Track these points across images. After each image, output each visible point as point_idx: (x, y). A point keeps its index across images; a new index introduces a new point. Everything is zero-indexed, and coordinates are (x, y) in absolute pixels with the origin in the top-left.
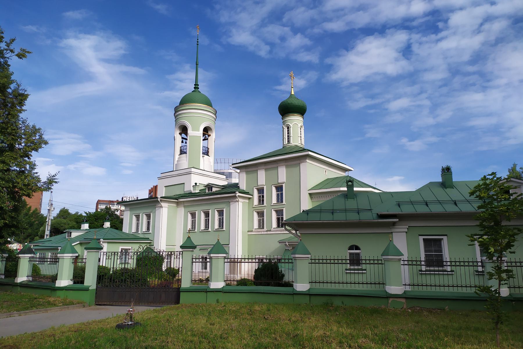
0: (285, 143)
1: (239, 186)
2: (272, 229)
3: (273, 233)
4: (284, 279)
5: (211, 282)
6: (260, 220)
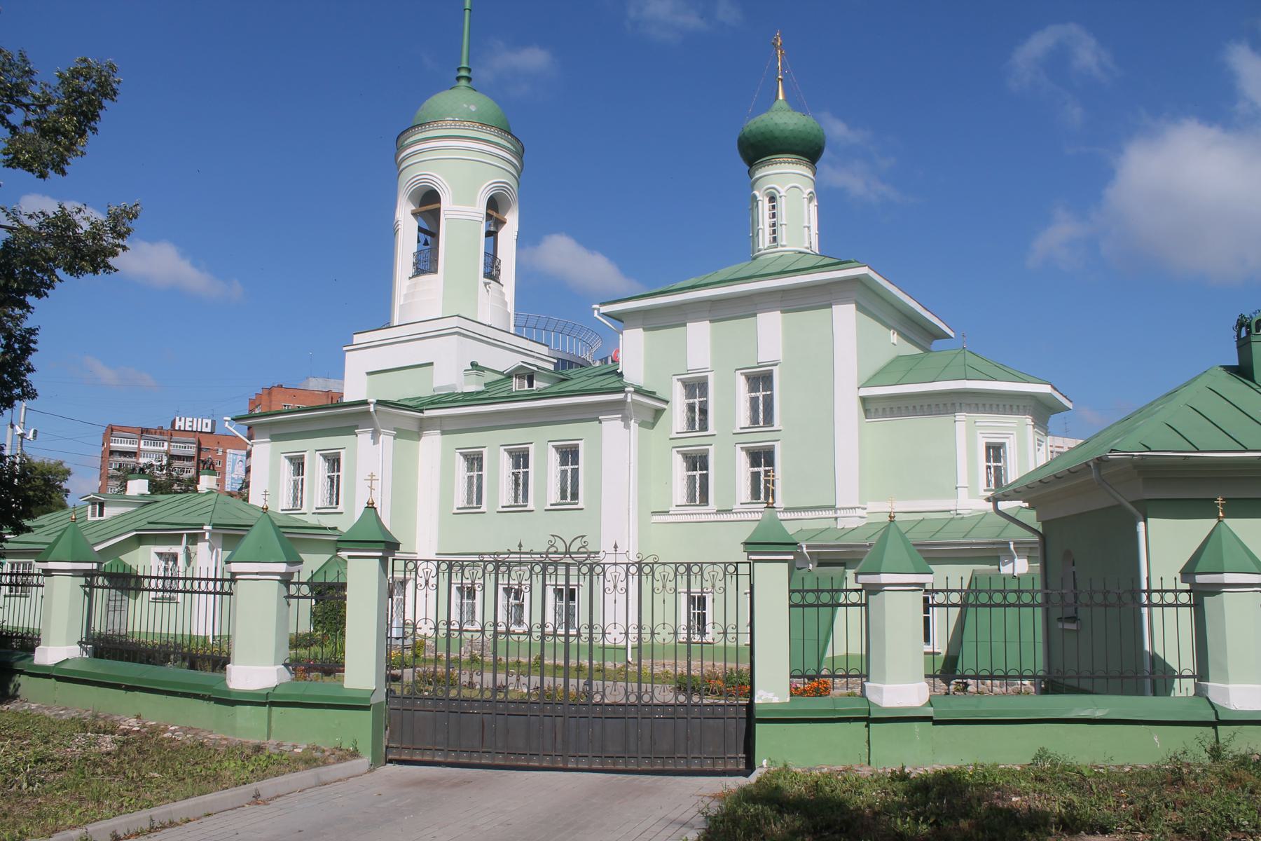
0: (764, 245)
1: (621, 373)
2: (673, 509)
3: (738, 517)
4: (959, 667)
5: (882, 680)
6: (691, 478)
